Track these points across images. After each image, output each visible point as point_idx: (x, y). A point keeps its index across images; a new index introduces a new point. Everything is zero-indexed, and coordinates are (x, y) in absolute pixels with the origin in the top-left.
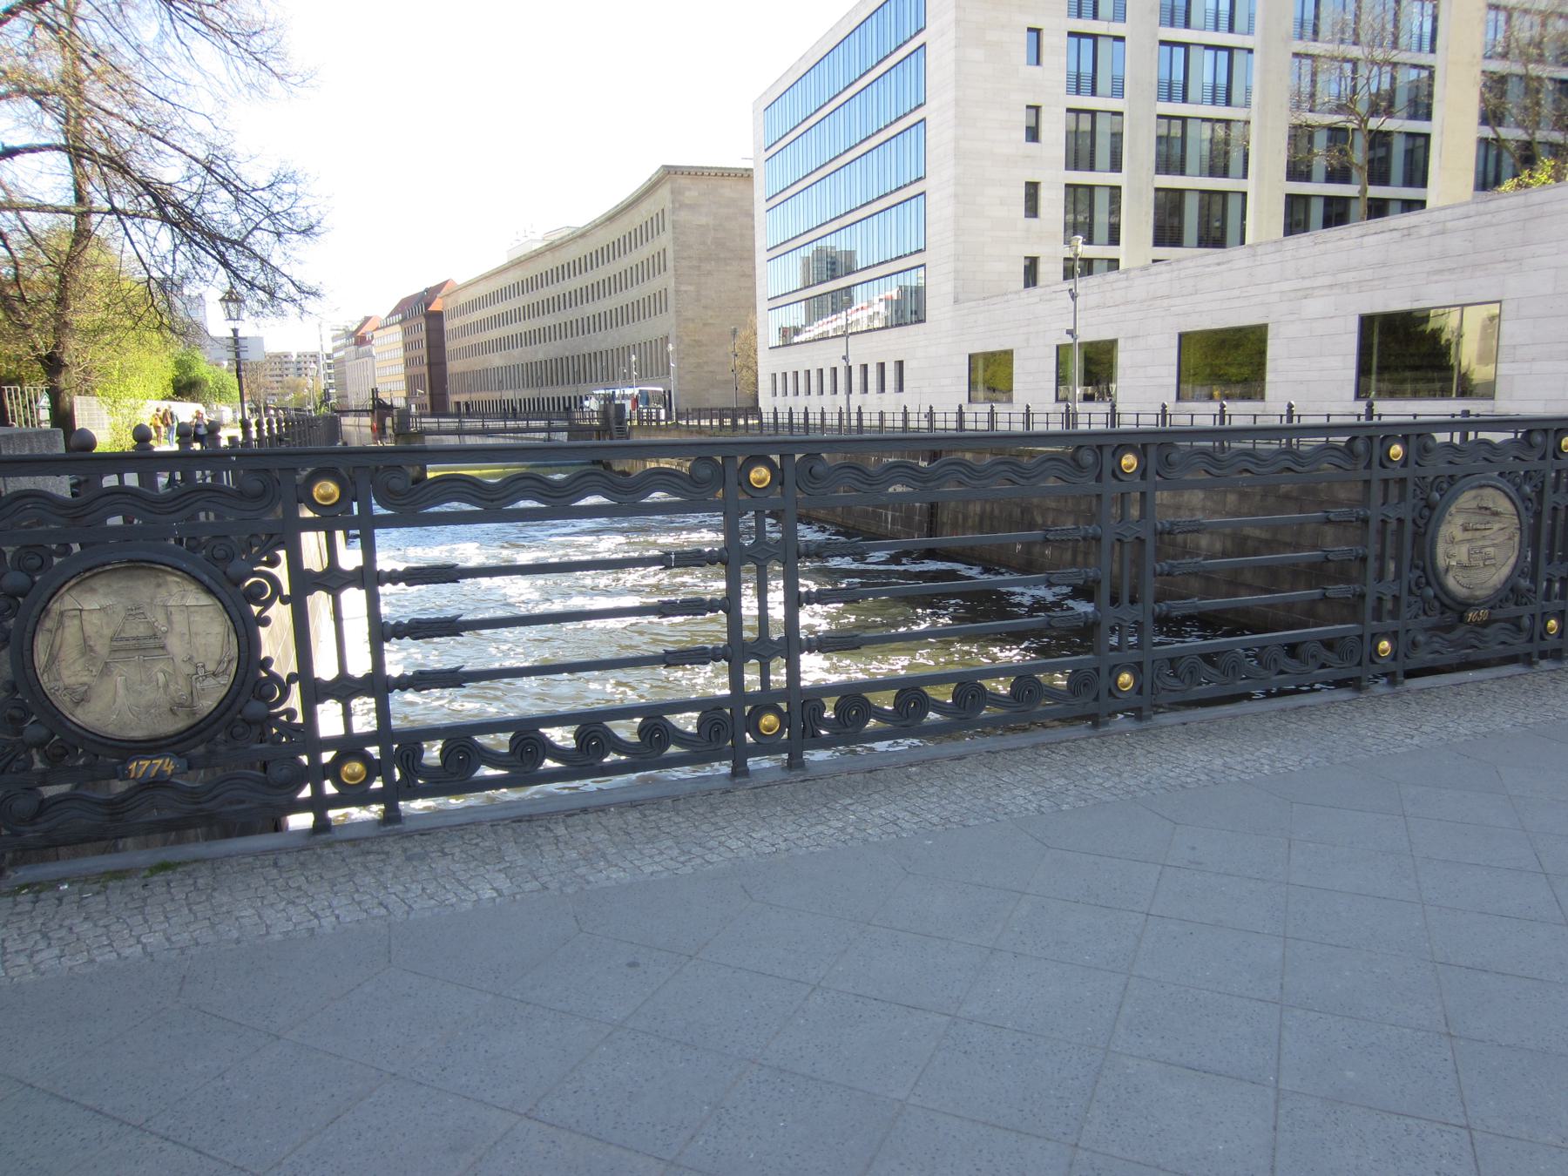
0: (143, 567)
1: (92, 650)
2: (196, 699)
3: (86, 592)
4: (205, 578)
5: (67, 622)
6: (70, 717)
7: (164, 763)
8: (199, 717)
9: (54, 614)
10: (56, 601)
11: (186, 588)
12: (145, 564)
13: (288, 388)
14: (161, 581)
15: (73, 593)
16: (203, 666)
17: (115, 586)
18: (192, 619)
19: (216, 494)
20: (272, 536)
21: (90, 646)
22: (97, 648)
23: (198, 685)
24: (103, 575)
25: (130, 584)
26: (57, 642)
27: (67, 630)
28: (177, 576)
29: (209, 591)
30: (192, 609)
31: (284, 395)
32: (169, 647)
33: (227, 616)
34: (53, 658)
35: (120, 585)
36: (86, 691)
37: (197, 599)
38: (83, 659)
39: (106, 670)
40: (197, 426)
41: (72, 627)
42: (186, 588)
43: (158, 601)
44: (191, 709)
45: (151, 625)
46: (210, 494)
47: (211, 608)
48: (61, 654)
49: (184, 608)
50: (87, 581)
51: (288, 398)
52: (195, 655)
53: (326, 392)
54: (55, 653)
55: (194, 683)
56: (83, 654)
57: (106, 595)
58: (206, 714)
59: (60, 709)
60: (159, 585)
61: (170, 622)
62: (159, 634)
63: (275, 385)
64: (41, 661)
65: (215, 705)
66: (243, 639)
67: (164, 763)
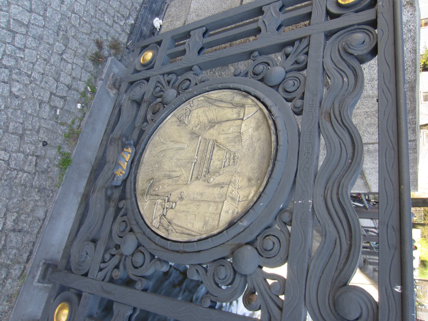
0: (269, 166)
1: (212, 127)
2: (152, 198)
3: (257, 123)
4: (245, 223)
5: (235, 110)
6: (172, 114)
7: (123, 170)
8: (139, 197)
9: (244, 101)
10: (253, 101)
11: (241, 204)
12: (270, 168)
13: (424, 294)
14: (253, 182)
15: (258, 114)
16: (172, 208)
17: (257, 145)
18: (212, 204)
19: (344, 256)
20: (281, 309)
21: (215, 126)
22: (211, 130)
23: (160, 201)
24: (268, 134)
25: (257, 157)
26: (223, 105)
27: (230, 110)
28: (253, 197)
29: (231, 224)
30: (220, 205)
31: (422, 291)
32: (196, 182)
33: (204, 236)
34: (211, 102)
35: (257, 148)
36: (185, 123)
37: (227, 212)
38: (206, 121)
39: (194, 135)
40: (3, 263)
41: (231, 113)
42: (241, 204)
43: (237, 178)
44: (145, 193)
45: (217, 172)
46: (345, 247)
47: (217, 222)
48: (214, 107)
49: (223, 199)
50: (266, 123)
51: (420, 293)
52: (184, 202)
53: (423, 305)
54: (216, 104)
55: (162, 198)
56: (210, 122)
57: (251, 138)
58: (139, 204)
59: (179, 108)
60: (249, 180)
61: (215, 186)
62: (208, 176)
63: (425, 290)
64: (212, 95)
65: (142, 212)
66: (181, 247)
67: (123, 170)
